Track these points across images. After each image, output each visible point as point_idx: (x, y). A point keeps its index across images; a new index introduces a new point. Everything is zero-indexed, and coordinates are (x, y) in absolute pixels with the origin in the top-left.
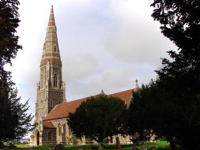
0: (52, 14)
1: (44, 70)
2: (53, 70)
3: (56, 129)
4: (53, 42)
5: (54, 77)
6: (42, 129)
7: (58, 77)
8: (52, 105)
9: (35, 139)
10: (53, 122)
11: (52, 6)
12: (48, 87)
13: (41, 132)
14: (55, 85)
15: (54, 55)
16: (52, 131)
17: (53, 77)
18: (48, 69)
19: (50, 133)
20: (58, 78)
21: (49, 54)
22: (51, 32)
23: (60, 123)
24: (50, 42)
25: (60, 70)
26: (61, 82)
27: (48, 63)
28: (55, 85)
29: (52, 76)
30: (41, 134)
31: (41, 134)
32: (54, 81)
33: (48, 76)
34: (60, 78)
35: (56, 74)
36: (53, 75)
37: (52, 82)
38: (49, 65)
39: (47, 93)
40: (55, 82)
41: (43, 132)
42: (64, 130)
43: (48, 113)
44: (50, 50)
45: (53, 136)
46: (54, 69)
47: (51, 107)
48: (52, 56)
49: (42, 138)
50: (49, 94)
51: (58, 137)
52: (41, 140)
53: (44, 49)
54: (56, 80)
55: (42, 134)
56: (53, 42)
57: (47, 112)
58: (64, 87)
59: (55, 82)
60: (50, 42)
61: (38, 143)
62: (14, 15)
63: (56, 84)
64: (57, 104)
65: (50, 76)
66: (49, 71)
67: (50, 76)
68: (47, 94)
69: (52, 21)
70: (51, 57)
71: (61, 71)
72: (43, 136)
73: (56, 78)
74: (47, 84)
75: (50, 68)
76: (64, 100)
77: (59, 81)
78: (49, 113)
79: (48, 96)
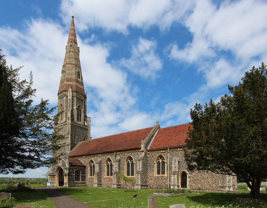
0: (72, 27)
1: (65, 98)
2: (76, 100)
3: (85, 167)
4: (75, 64)
5: (78, 110)
6: (67, 166)
7: (82, 110)
8: (75, 142)
9: (56, 178)
10: (80, 160)
11: (73, 17)
12: (70, 119)
13: (67, 169)
14: (79, 119)
15: (77, 81)
16: (81, 169)
17: (76, 109)
18: (70, 97)
19: (77, 173)
20: (82, 112)
21: (71, 78)
22: (72, 52)
23: (91, 160)
24: (72, 64)
25: (85, 103)
26: (85, 116)
27: (70, 90)
28: (79, 119)
29: (75, 108)
30: (66, 172)
31: (66, 172)
32: (78, 114)
33: (70, 106)
34: (85, 112)
35: (79, 106)
36: (76, 106)
37: (75, 115)
38: (71, 92)
39: (70, 125)
40: (79, 115)
41: (69, 169)
42: (100, 168)
43: (71, 150)
44: (72, 74)
45: (81, 176)
46: (78, 99)
47: (75, 143)
48: (75, 83)
49: (68, 178)
50: (71, 128)
51: (88, 177)
52: (66, 180)
53: (63, 72)
54: (80, 113)
55: (68, 172)
56: (75, 64)
57: (70, 148)
58: (89, 123)
59: (79, 115)
60: (72, 64)
61: (61, 183)
62: (36, 148)
63: (80, 118)
64: (81, 141)
65: (72, 107)
66: (71, 100)
67: (72, 107)
68: (70, 127)
69: (73, 38)
70: (74, 83)
71: (85, 104)
72: (69, 175)
73: (80, 111)
74: (69, 115)
75: (72, 97)
76: (90, 138)
77: (84, 115)
78: (73, 150)
79: (70, 129)
